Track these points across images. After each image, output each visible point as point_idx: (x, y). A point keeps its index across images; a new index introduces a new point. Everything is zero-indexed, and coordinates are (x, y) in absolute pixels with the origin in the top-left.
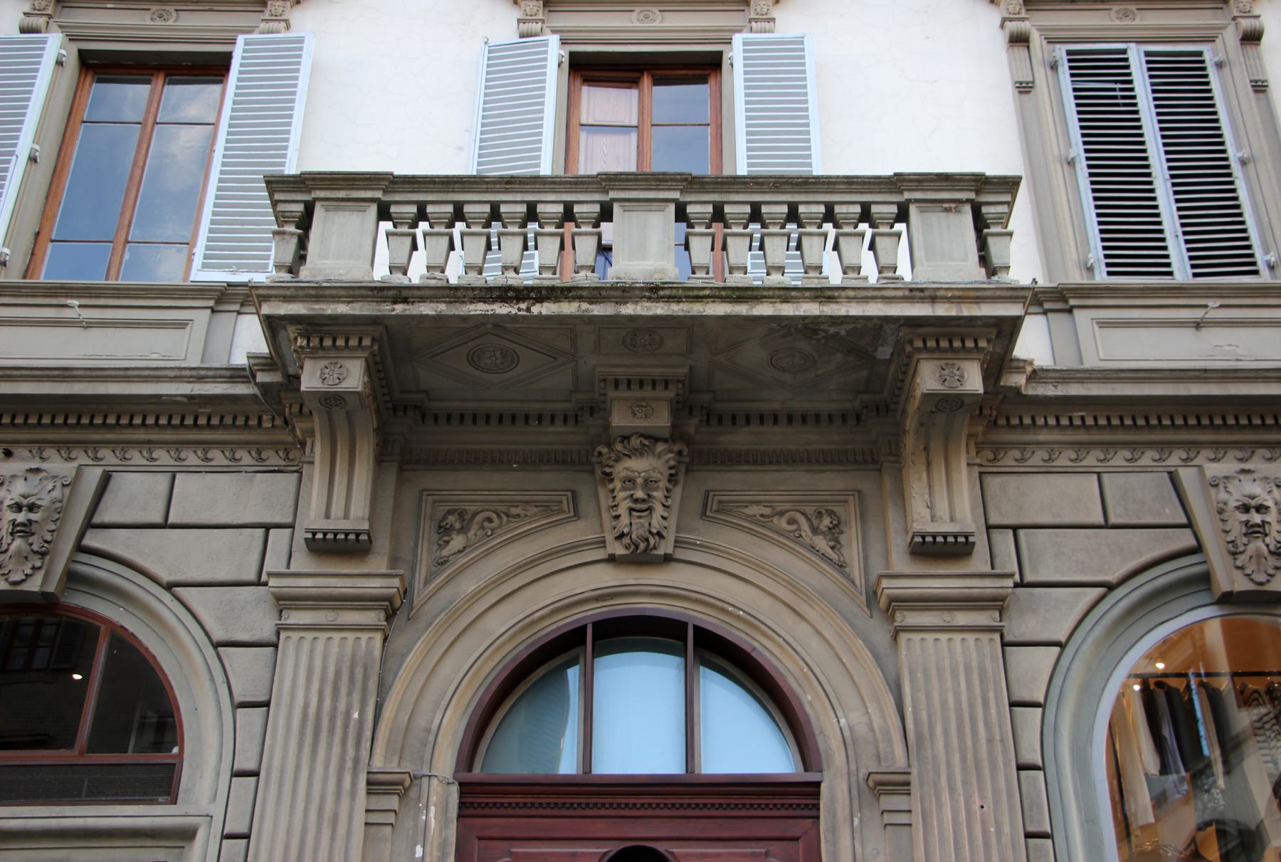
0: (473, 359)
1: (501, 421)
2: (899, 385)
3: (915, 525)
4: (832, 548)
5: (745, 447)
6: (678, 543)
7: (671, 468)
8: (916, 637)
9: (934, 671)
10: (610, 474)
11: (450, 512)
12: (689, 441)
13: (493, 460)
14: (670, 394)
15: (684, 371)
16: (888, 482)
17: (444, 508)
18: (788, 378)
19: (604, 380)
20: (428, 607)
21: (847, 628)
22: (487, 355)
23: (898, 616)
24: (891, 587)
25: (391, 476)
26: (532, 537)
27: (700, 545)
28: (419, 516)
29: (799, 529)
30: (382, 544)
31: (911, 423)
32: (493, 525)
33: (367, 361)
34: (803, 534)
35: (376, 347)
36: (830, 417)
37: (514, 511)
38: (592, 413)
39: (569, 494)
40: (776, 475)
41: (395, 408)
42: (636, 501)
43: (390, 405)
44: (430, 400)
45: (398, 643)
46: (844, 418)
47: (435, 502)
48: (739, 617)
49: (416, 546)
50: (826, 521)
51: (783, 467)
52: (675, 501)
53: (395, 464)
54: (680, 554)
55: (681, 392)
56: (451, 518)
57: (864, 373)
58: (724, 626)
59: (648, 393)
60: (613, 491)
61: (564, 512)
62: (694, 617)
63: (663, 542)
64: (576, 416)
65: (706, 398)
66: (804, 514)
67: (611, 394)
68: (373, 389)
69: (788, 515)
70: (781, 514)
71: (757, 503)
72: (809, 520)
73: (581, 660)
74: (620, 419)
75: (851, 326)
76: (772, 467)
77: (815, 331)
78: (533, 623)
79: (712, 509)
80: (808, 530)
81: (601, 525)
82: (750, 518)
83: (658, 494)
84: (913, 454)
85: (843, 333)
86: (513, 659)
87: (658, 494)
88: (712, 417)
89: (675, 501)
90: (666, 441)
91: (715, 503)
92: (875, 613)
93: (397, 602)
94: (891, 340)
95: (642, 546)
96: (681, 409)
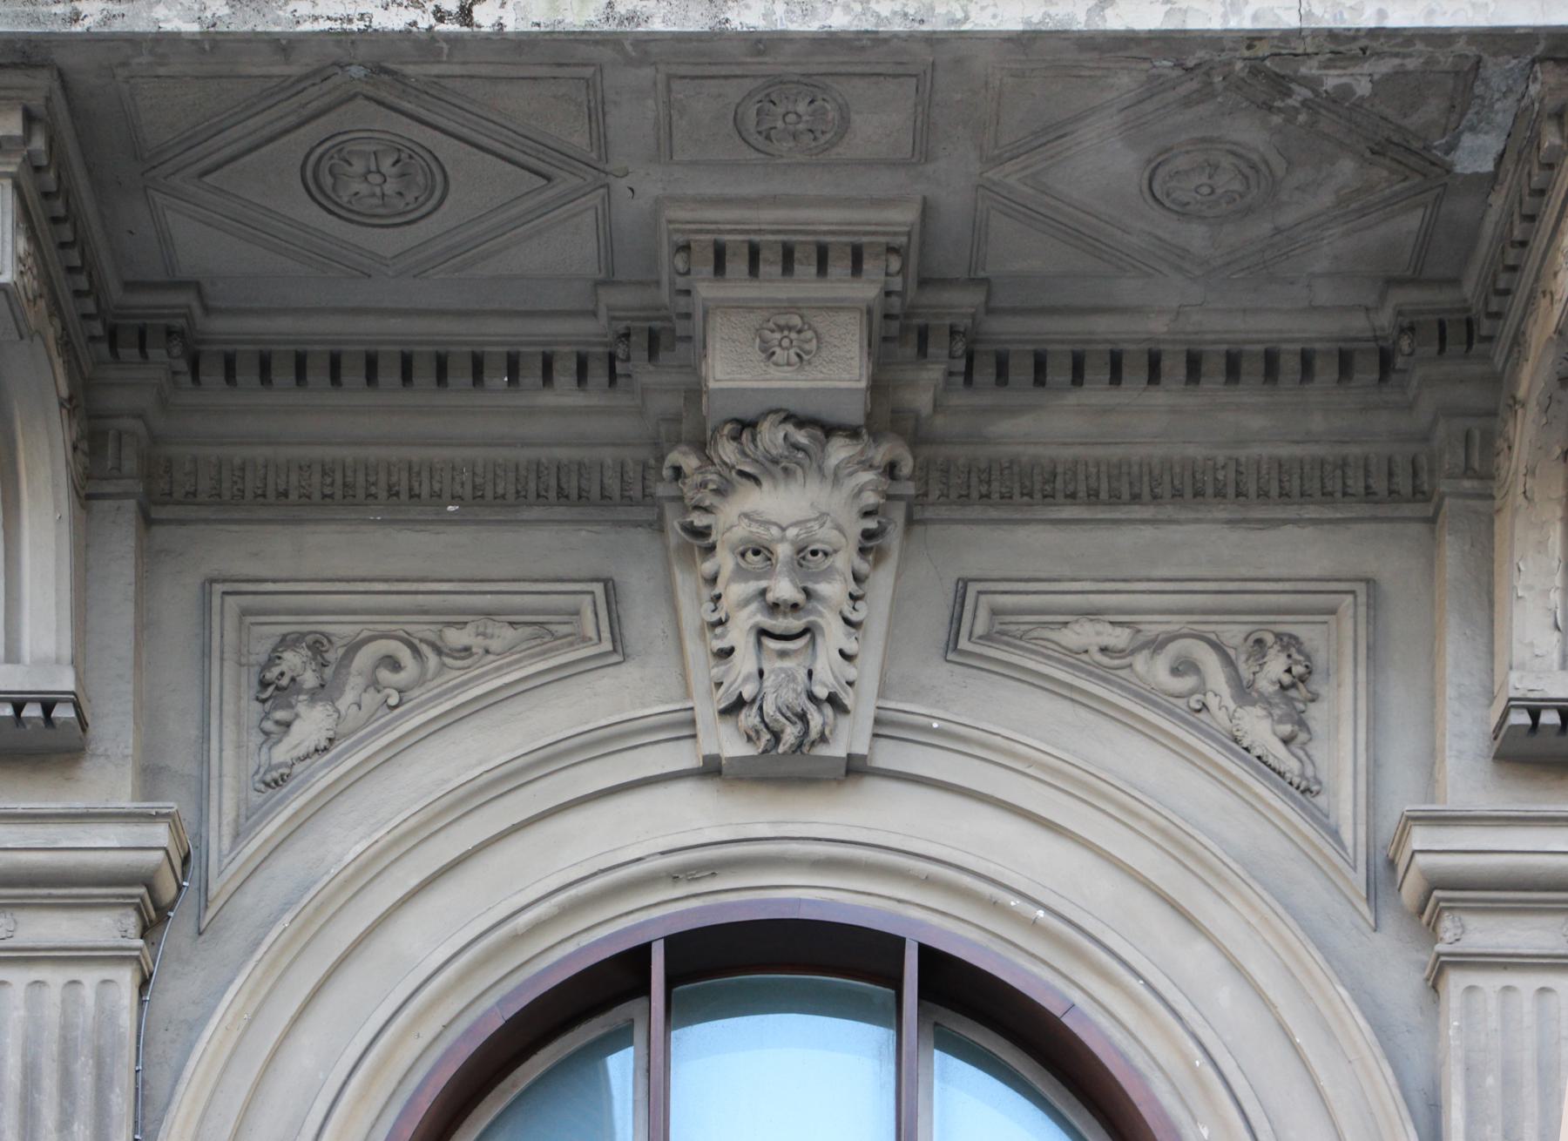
0: (317, 182)
1: (407, 376)
2: (1511, 257)
3: (1514, 677)
4: (1286, 741)
5: (1068, 453)
6: (883, 727)
7: (867, 514)
8: (1490, 983)
9: (1529, 1074)
10: (702, 533)
11: (286, 642)
12: (917, 439)
13: (393, 493)
14: (867, 290)
15: (903, 217)
16: (1452, 553)
17: (266, 635)
18: (1195, 236)
19: (686, 248)
20: (247, 899)
21: (1313, 959)
22: (358, 166)
23: (1448, 925)
24: (1435, 849)
25: (121, 537)
26: (496, 714)
27: (939, 732)
28: (206, 653)
29: (1201, 688)
30: (115, 730)
31: (1533, 377)
32: (401, 678)
33: (17, 187)
34: (1212, 702)
35: (39, 143)
36: (1307, 360)
37: (455, 638)
38: (653, 353)
39: (598, 588)
40: (1148, 532)
41: (112, 336)
42: (774, 608)
43: (98, 328)
44: (207, 310)
45: (174, 993)
46: (1345, 363)
47: (245, 612)
48: (1034, 926)
49: (205, 738)
50: (1276, 666)
51: (1169, 511)
52: (875, 611)
53: (131, 504)
54: (888, 756)
55: (897, 284)
56: (292, 660)
57: (1412, 221)
58: (997, 947)
59: (805, 286)
60: (713, 580)
61: (585, 640)
62: (920, 924)
63: (844, 722)
64: (612, 358)
65: (965, 301)
66: (1217, 647)
67: (707, 290)
68: (46, 278)
69: (1173, 649)
70: (1156, 645)
71: (1092, 613)
72: (1228, 662)
73: (639, 1034)
74: (732, 368)
75: (1385, 67)
76: (1138, 512)
77: (1281, 84)
78: (517, 938)
79: (972, 631)
80: (1225, 691)
81: (684, 676)
82: (1073, 658)
83: (833, 590)
84: (1531, 472)
85: (1363, 88)
86: (470, 1032)
87: (833, 590)
88: (983, 362)
89: (875, 611)
90: (853, 433)
91: (983, 615)
92: (1389, 920)
93: (168, 889)
94: (1503, 112)
95: (791, 733)
96: (899, 335)
